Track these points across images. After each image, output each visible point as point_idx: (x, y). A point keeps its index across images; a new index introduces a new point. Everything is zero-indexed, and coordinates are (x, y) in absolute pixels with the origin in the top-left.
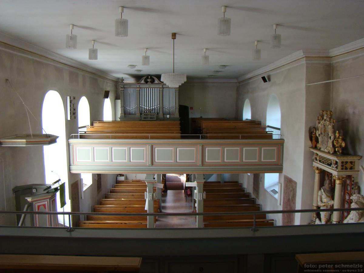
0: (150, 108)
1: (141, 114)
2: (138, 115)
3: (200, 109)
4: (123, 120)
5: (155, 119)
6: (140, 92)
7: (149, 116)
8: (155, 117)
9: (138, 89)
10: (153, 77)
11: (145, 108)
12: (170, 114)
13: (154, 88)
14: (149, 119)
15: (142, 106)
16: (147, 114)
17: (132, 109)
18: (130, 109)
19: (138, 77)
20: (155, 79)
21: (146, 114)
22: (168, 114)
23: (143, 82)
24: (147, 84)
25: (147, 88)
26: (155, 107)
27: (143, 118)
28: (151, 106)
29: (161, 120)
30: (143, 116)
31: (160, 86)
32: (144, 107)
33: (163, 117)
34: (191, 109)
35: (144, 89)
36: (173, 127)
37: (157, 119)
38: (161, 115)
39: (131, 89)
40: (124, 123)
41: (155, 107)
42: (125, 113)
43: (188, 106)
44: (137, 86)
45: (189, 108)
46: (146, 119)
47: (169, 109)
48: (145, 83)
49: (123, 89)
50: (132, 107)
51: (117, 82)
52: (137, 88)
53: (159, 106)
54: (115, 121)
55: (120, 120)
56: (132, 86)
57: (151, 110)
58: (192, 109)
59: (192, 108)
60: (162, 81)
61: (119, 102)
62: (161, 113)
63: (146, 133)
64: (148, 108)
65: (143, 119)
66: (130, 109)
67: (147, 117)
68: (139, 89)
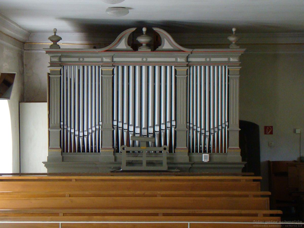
0: (144, 132)
1: (118, 151)
2: (107, 152)
3: (298, 131)
4: (62, 171)
5: (165, 167)
6: (113, 78)
7: (144, 159)
8: (165, 161)
9: (104, 69)
10: (155, 29)
11: (128, 131)
12: (209, 151)
13: (160, 64)
14: (144, 167)
15: (120, 125)
16: (155, 149)
17: (86, 133)
18: (81, 134)
19: (100, 33)
20: (162, 36)
21: (131, 149)
22: (205, 152)
23: (123, 45)
24: (135, 54)
25: (134, 65)
26: (163, 127)
27: (124, 163)
28: (150, 124)
29: (182, 171)
30: (123, 157)
31: (179, 60)
32: (125, 127)
33: (187, 161)
34: (265, 133)
35: (137, 68)
36: (247, 196)
37: (169, 168)
38: (181, 155)
39: (69, 66)
40: (76, 180)
41: (163, 127)
42: (65, 148)
43: (259, 124)
44: (105, 60)
45: (262, 130)
46: (133, 168)
47: (207, 134)
48: (129, 48)
49: (58, 69)
50: (88, 126)
51: (24, 43)
52: (106, 65)
53: (174, 123)
54: (20, 174)
55: (45, 170)
56: (86, 60)
57: (150, 136)
58: (271, 133)
59: (269, 130)
60: (57, 35)
61: (39, 113)
62: (182, 146)
63: (164, 215)
64: (138, 131)
65: (124, 167)
66: (81, 134)
67: (137, 159)
68: (111, 69)
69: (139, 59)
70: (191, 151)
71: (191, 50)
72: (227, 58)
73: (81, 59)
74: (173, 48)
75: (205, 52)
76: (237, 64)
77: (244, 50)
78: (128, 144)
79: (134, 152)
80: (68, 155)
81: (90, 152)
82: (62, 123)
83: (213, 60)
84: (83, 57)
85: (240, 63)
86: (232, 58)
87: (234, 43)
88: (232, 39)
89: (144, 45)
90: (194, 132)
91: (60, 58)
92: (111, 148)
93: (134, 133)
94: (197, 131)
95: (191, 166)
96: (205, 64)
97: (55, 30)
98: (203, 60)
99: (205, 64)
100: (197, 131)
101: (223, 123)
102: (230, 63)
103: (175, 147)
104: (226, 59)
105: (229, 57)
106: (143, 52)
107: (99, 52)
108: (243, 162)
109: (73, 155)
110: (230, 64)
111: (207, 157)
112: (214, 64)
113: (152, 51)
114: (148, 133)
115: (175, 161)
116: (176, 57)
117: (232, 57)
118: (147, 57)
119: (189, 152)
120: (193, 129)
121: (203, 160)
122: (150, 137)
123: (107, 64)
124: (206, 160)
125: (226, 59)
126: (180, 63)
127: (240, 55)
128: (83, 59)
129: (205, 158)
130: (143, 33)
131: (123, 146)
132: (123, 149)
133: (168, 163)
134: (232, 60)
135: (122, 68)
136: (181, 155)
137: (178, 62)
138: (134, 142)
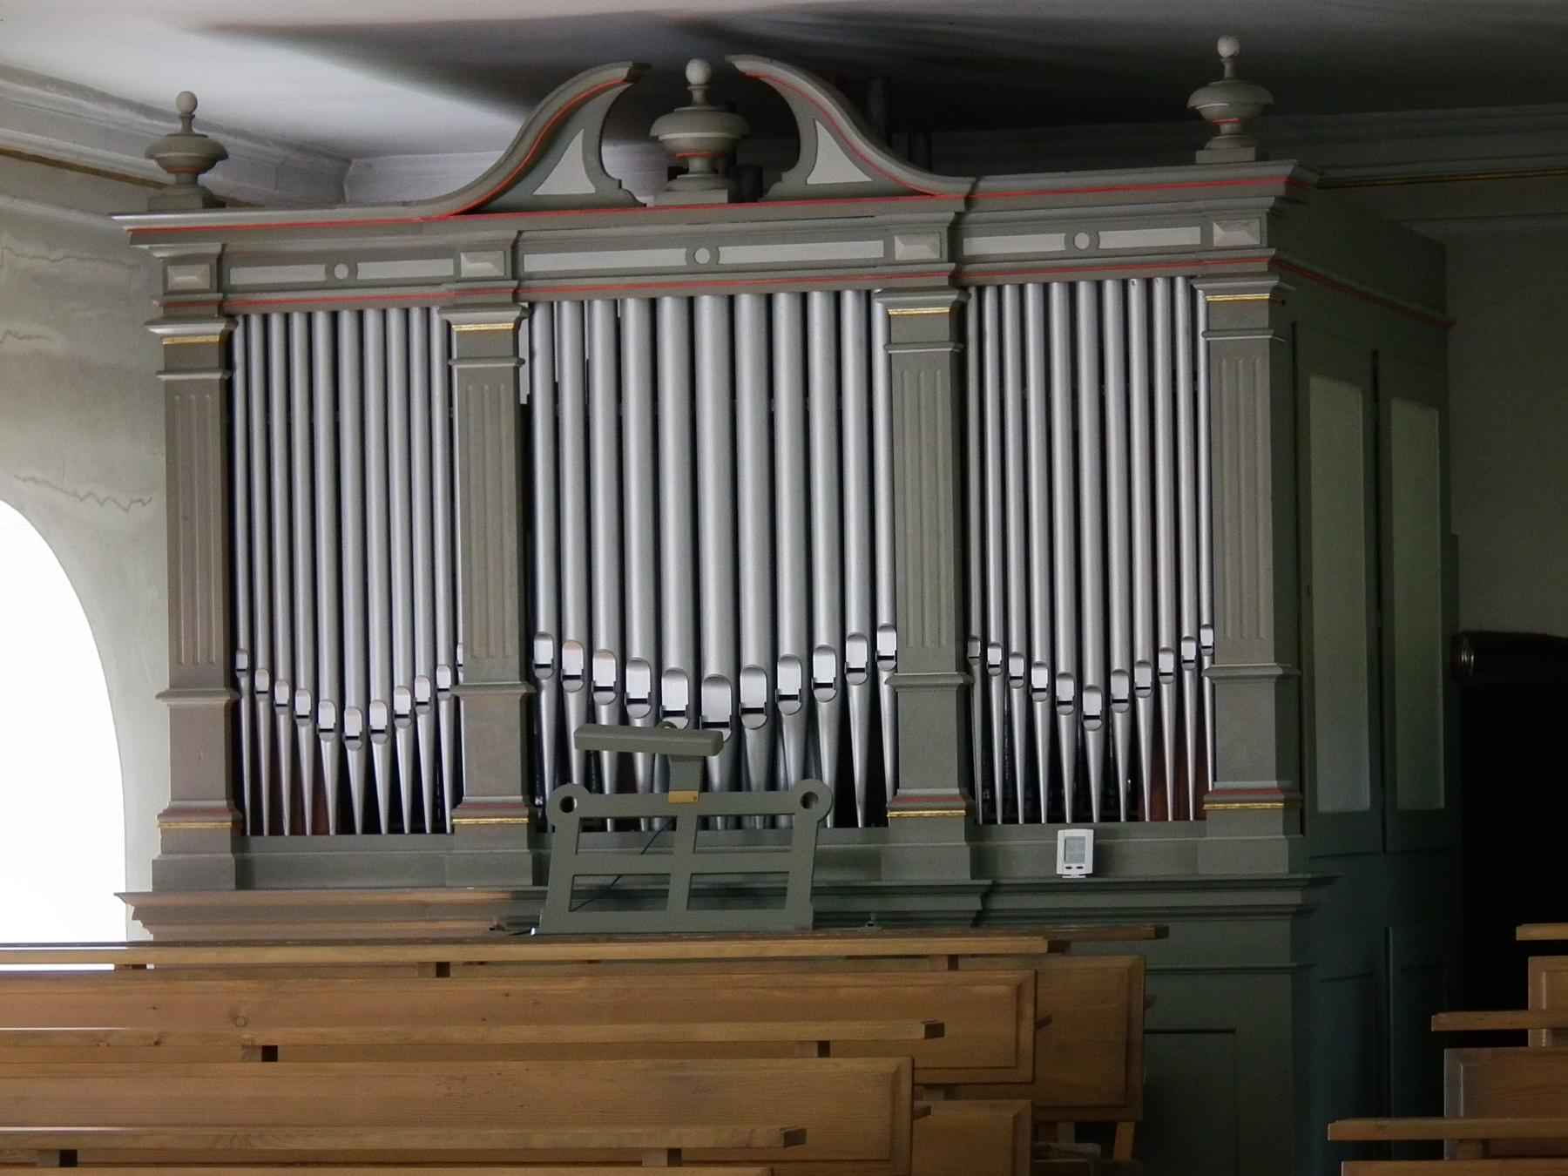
9: (466, 324)
16: (737, 803)
17: (379, 718)
21: (609, 803)
32: (605, 672)
35: (784, 307)
38: (928, 831)
47: (1093, 703)
49: (502, 321)
50: (389, 672)
52: (473, 295)
56: (368, 271)
66: (353, 726)
69: (674, 257)
70: (985, 813)
71: (961, 185)
72: (1197, 230)
73: (342, 272)
74: (868, 179)
75: (1124, 188)
76: (1255, 259)
77: (1283, 169)
78: (592, 778)
79: (738, 822)
80: (263, 848)
81: (428, 829)
82: (242, 661)
83: (1113, 240)
84: (352, 259)
85: (1273, 252)
86: (1223, 227)
87: (1226, 128)
88: (1210, 103)
89: (696, 164)
90: (1016, 694)
91: (220, 264)
92: (514, 805)
93: (623, 701)
94: (1029, 691)
95: (979, 907)
96: (1065, 271)
97: (186, 106)
98: (1051, 243)
99: (1065, 271)
100: (1029, 691)
101: (1186, 633)
102: (1211, 255)
103: (896, 785)
104: (1187, 236)
105: (1203, 219)
106: (684, 207)
107: (427, 219)
108: (976, 882)
109: (308, 847)
110: (1215, 262)
111: (1083, 848)
112: (1125, 266)
113: (735, 198)
114: (739, 710)
115: (887, 879)
116: (884, 232)
117: (1228, 216)
118: (715, 242)
119: (238, 828)
120: (1007, 679)
121: (1061, 869)
122: (638, 723)
123: (1232, 261)
124: (1074, 866)
125: (1187, 236)
126: (1226, 255)
127: (1271, 201)
128: (354, 271)
129: (1073, 851)
130: (690, 94)
131: (565, 791)
132: (567, 805)
133: (816, 892)
134: (1220, 236)
135: (763, 304)
136: (928, 831)
137: (898, 264)
138: (625, 763)
